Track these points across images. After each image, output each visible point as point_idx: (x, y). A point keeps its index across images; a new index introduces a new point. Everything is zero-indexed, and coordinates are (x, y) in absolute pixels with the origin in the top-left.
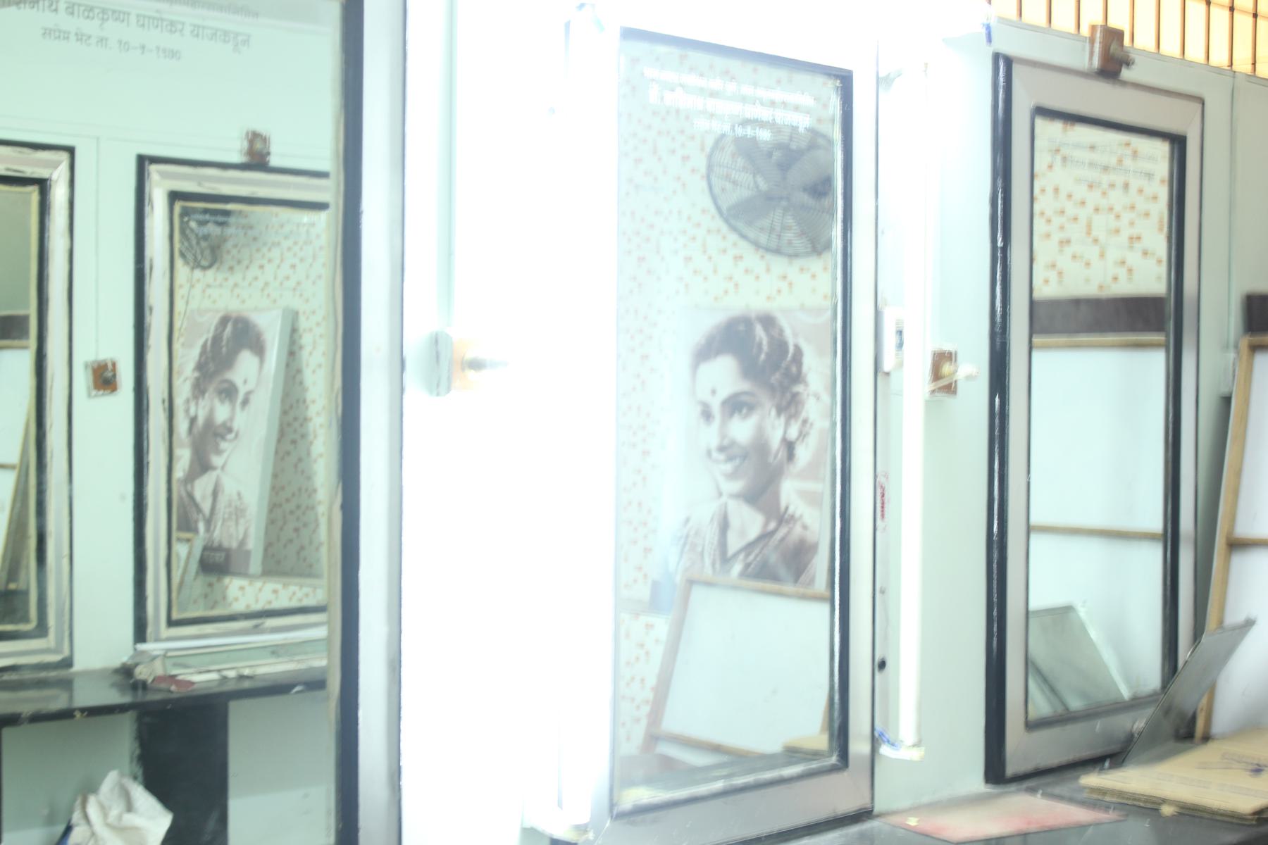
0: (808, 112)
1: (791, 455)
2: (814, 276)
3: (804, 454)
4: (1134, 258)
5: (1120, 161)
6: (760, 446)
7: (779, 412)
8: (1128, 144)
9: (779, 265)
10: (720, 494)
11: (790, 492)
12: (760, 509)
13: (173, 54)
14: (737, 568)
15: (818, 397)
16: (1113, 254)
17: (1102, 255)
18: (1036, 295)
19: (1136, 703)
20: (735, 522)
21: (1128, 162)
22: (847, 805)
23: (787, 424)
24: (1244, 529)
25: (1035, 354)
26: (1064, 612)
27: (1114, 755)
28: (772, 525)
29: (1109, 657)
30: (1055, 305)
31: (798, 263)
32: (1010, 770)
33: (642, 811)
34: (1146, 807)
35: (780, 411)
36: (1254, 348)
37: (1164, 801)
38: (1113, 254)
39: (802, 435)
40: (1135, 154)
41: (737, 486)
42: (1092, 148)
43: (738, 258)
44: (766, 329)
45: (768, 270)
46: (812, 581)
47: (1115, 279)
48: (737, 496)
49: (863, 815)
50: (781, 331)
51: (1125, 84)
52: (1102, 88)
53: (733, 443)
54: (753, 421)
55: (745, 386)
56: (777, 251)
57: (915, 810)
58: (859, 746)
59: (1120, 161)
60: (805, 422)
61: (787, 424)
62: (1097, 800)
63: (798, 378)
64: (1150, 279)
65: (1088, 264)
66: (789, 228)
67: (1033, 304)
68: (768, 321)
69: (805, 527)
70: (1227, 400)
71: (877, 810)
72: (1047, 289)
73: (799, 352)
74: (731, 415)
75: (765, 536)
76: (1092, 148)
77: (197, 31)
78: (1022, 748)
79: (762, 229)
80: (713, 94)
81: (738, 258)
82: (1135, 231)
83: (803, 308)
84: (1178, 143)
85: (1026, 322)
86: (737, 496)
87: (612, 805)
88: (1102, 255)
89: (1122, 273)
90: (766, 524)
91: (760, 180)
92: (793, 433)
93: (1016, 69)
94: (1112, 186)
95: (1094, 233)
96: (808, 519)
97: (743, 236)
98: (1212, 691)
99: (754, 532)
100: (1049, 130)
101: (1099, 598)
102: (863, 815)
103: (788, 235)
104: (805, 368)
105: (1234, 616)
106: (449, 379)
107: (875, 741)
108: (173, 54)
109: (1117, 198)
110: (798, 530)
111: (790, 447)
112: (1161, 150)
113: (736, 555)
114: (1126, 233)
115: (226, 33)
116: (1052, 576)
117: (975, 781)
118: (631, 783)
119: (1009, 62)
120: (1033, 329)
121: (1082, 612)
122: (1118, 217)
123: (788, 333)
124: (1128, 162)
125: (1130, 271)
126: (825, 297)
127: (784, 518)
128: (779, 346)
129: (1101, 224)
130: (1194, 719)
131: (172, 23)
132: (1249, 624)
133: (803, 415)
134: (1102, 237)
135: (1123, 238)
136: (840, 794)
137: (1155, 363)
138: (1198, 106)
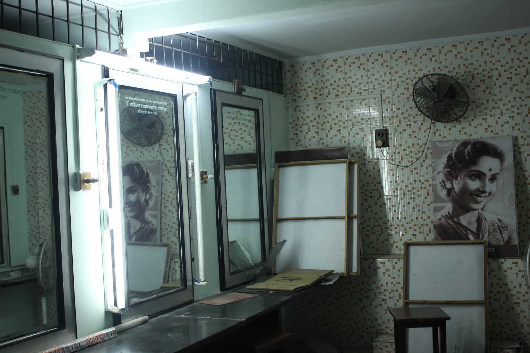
0: (165, 106)
1: (147, 204)
2: (150, 152)
3: (151, 203)
4: (242, 143)
5: (237, 116)
6: (138, 201)
7: (143, 193)
8: (239, 112)
9: (140, 149)
10: (127, 217)
11: (148, 215)
12: (139, 221)
13: (5, 97)
14: (134, 239)
15: (154, 187)
16: (237, 142)
17: (234, 143)
18: (225, 154)
19: (256, 266)
20: (132, 225)
21: (239, 117)
22: (187, 300)
23: (146, 195)
24: (280, 216)
25: (226, 171)
26: (235, 242)
27: (253, 280)
28: (143, 225)
29: (247, 254)
30: (229, 156)
31: (145, 148)
32: (227, 287)
33: (136, 304)
34: (266, 291)
35: (143, 192)
36: (280, 167)
37: (270, 290)
38: (237, 142)
39: (150, 198)
40: (241, 114)
41: (132, 214)
42: (229, 113)
43: (128, 147)
44: (137, 168)
45: (137, 150)
46: (156, 240)
47: (238, 149)
48: (131, 217)
49: (192, 301)
50: (142, 168)
51: (243, 96)
52: (238, 97)
53: (131, 202)
54: (136, 195)
55: (133, 185)
56: (139, 145)
57: (205, 299)
58: (189, 283)
59: (237, 116)
60: (151, 194)
61: (146, 195)
62: (251, 291)
63: (148, 181)
64: (249, 147)
65: (230, 145)
66: (142, 138)
67: (225, 156)
68: (138, 165)
69: (153, 225)
70: (273, 181)
71: (195, 299)
72: (227, 152)
73: (148, 174)
74: (129, 194)
75: (141, 228)
76: (229, 113)
77: (10, 91)
78: (229, 280)
79: (134, 138)
80: (141, 103)
81: (128, 147)
82: (242, 136)
83: (147, 161)
84: (257, 111)
85: (224, 161)
86: (131, 217)
87: (128, 305)
88: (234, 143)
89: (239, 147)
90: (141, 225)
91: (134, 123)
92: (148, 197)
93: (217, 92)
94: (235, 123)
95: (231, 137)
96: (153, 223)
97: (130, 140)
98: (275, 262)
99: (138, 227)
100: (226, 109)
101: (245, 237)
102: (192, 301)
103: (142, 140)
104: (150, 179)
105: (280, 240)
106: (80, 186)
107: (193, 280)
108: (5, 97)
109: (237, 127)
110: (151, 225)
111: (147, 201)
112: (252, 113)
113: (134, 234)
114: (240, 136)
115: (18, 91)
116: (234, 232)
117: (218, 291)
118: (133, 297)
119: (215, 91)
120: (225, 164)
121: (238, 242)
122: (237, 132)
123: (144, 168)
124: (239, 117)
125: (242, 147)
126: (171, 157)
127: (147, 223)
128: (142, 172)
129: (34, 116)
130: (271, 269)
131: (4, 89)
132: (285, 241)
133: (150, 192)
134: (233, 137)
135: (239, 138)
136: (185, 297)
137: (254, 172)
138: (62, 61)
